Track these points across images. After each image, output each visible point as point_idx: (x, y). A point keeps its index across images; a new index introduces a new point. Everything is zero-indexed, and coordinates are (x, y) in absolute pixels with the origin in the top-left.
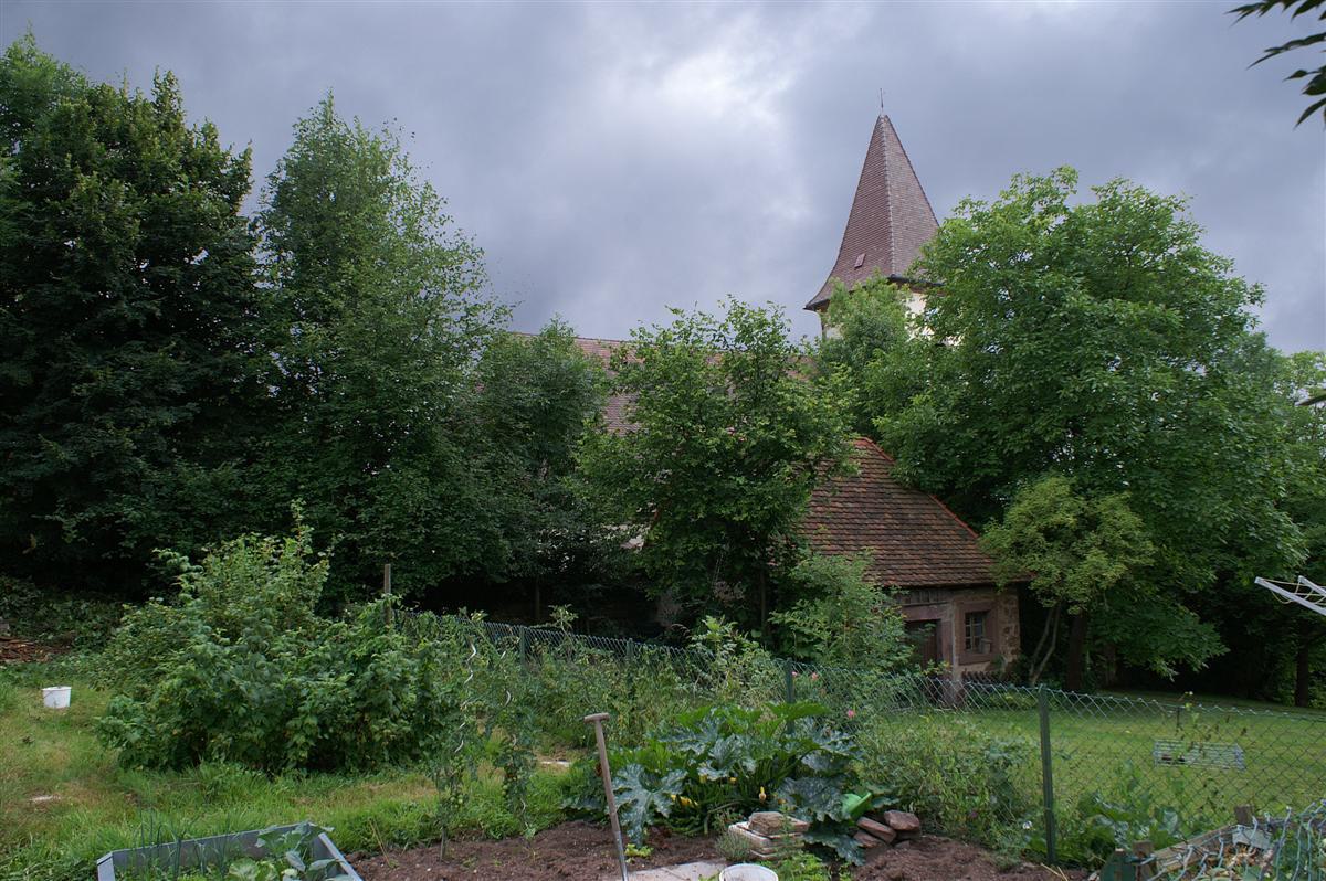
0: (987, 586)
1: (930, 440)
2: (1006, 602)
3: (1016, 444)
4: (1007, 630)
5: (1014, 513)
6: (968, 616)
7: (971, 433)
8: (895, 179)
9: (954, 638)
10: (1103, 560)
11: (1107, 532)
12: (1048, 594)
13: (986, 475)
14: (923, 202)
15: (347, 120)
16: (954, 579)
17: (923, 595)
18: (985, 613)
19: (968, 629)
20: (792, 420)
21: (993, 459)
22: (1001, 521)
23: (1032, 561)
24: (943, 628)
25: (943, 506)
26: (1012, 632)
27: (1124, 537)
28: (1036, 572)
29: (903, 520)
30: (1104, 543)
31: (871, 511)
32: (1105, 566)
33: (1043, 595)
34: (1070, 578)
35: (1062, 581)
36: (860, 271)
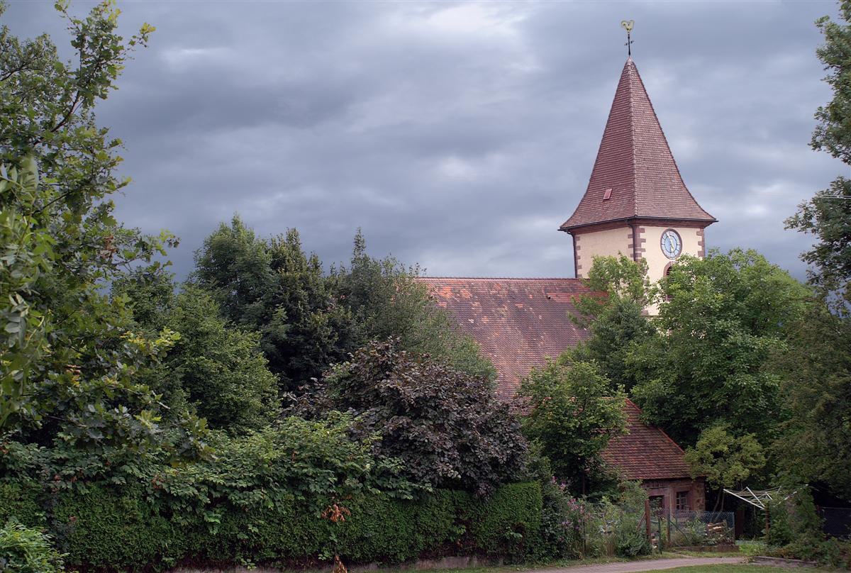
0: (687, 479)
1: (661, 401)
2: (698, 486)
3: (703, 404)
4: (698, 501)
5: (701, 443)
6: (678, 493)
7: (682, 397)
8: (638, 125)
9: (671, 505)
10: (740, 467)
11: (744, 453)
12: (715, 484)
13: (689, 419)
14: (662, 142)
15: (375, 254)
16: (671, 475)
17: (655, 484)
18: (687, 492)
19: (678, 500)
20: (603, 416)
21: (693, 410)
22: (694, 448)
23: (707, 468)
24: (665, 499)
25: (666, 436)
26: (701, 502)
27: (752, 456)
28: (709, 473)
29: (646, 444)
30: (742, 459)
31: (630, 440)
32: (741, 470)
33: (712, 484)
34: (724, 476)
35: (721, 478)
36: (608, 204)
